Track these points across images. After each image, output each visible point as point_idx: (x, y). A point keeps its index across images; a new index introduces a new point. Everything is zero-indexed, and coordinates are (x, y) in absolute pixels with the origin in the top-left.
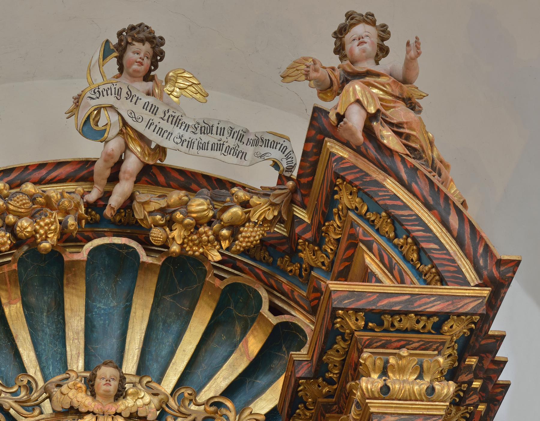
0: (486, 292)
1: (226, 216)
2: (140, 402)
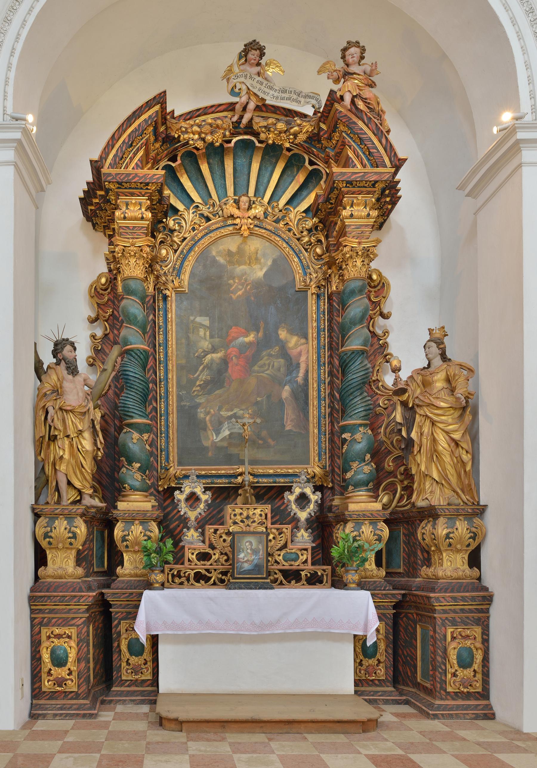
0: (393, 170)
1: (292, 131)
2: (257, 211)
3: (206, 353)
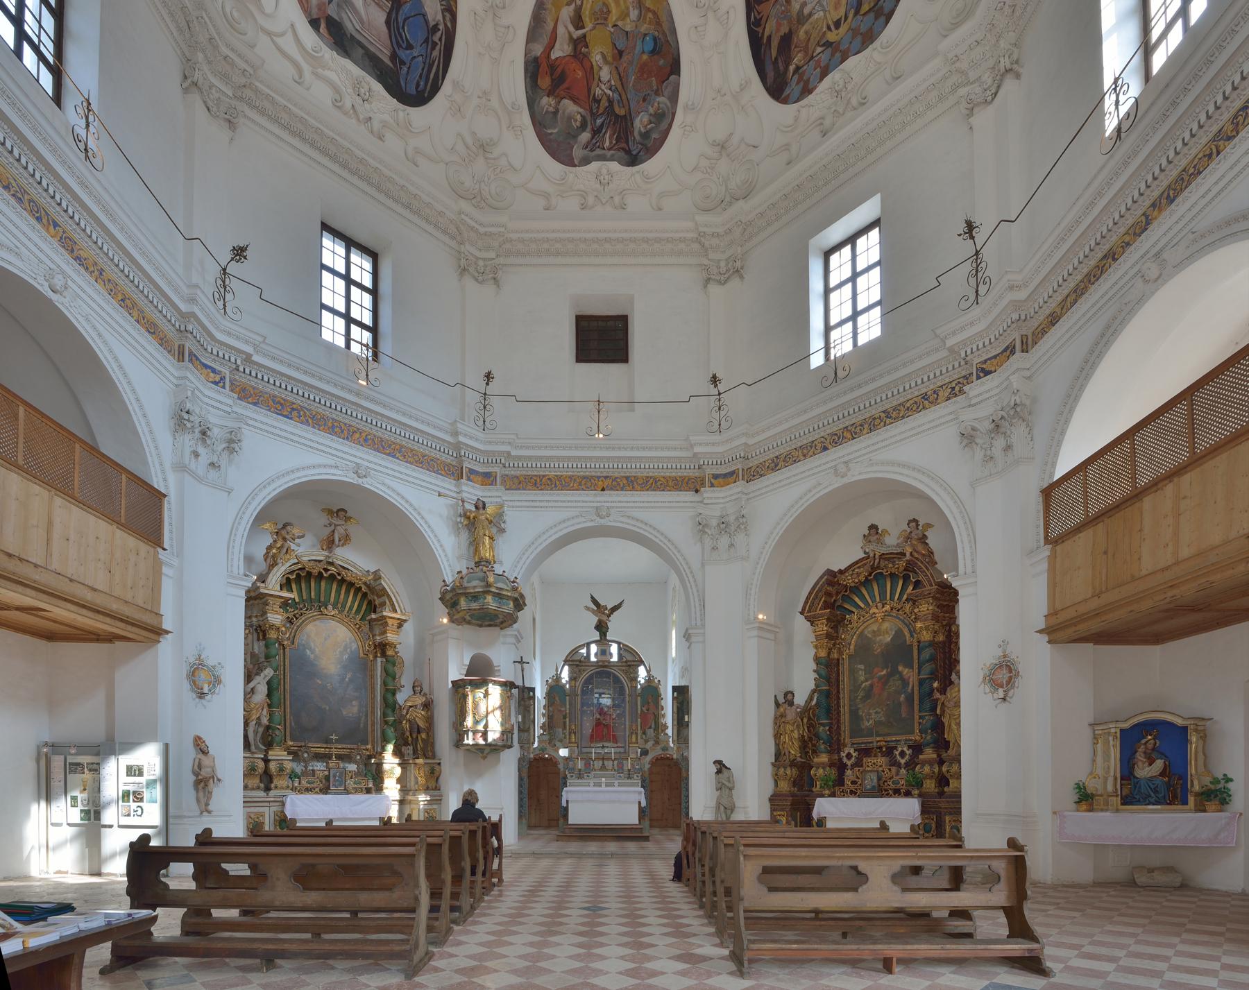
3: (862, 682)
